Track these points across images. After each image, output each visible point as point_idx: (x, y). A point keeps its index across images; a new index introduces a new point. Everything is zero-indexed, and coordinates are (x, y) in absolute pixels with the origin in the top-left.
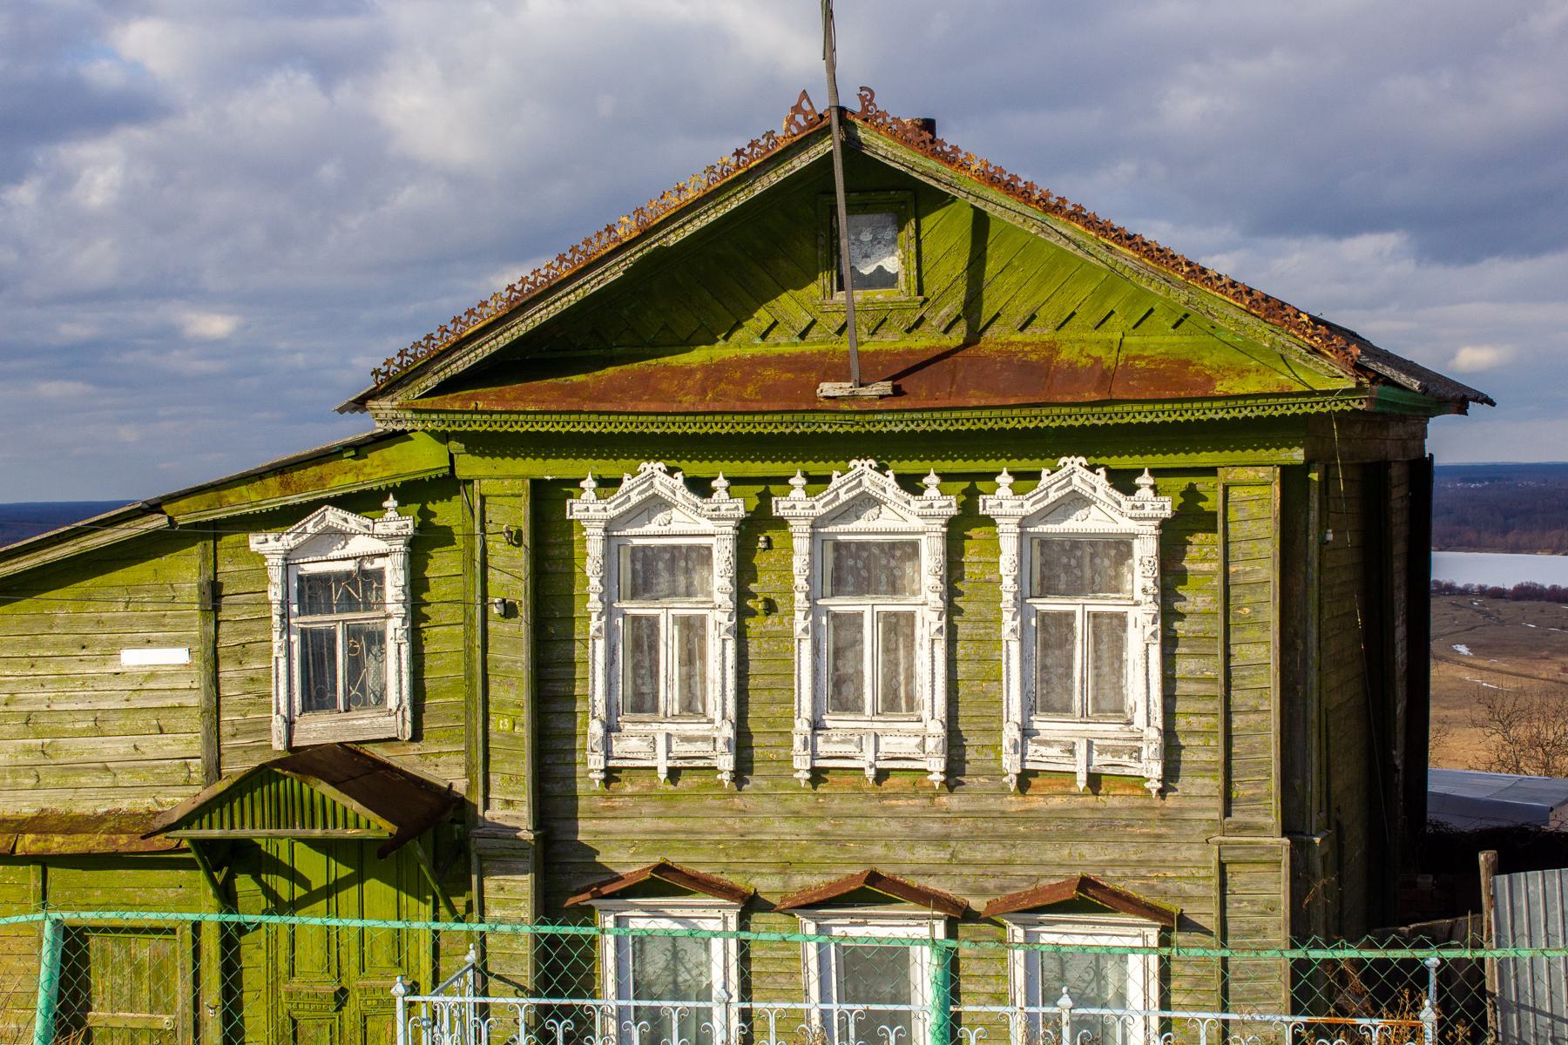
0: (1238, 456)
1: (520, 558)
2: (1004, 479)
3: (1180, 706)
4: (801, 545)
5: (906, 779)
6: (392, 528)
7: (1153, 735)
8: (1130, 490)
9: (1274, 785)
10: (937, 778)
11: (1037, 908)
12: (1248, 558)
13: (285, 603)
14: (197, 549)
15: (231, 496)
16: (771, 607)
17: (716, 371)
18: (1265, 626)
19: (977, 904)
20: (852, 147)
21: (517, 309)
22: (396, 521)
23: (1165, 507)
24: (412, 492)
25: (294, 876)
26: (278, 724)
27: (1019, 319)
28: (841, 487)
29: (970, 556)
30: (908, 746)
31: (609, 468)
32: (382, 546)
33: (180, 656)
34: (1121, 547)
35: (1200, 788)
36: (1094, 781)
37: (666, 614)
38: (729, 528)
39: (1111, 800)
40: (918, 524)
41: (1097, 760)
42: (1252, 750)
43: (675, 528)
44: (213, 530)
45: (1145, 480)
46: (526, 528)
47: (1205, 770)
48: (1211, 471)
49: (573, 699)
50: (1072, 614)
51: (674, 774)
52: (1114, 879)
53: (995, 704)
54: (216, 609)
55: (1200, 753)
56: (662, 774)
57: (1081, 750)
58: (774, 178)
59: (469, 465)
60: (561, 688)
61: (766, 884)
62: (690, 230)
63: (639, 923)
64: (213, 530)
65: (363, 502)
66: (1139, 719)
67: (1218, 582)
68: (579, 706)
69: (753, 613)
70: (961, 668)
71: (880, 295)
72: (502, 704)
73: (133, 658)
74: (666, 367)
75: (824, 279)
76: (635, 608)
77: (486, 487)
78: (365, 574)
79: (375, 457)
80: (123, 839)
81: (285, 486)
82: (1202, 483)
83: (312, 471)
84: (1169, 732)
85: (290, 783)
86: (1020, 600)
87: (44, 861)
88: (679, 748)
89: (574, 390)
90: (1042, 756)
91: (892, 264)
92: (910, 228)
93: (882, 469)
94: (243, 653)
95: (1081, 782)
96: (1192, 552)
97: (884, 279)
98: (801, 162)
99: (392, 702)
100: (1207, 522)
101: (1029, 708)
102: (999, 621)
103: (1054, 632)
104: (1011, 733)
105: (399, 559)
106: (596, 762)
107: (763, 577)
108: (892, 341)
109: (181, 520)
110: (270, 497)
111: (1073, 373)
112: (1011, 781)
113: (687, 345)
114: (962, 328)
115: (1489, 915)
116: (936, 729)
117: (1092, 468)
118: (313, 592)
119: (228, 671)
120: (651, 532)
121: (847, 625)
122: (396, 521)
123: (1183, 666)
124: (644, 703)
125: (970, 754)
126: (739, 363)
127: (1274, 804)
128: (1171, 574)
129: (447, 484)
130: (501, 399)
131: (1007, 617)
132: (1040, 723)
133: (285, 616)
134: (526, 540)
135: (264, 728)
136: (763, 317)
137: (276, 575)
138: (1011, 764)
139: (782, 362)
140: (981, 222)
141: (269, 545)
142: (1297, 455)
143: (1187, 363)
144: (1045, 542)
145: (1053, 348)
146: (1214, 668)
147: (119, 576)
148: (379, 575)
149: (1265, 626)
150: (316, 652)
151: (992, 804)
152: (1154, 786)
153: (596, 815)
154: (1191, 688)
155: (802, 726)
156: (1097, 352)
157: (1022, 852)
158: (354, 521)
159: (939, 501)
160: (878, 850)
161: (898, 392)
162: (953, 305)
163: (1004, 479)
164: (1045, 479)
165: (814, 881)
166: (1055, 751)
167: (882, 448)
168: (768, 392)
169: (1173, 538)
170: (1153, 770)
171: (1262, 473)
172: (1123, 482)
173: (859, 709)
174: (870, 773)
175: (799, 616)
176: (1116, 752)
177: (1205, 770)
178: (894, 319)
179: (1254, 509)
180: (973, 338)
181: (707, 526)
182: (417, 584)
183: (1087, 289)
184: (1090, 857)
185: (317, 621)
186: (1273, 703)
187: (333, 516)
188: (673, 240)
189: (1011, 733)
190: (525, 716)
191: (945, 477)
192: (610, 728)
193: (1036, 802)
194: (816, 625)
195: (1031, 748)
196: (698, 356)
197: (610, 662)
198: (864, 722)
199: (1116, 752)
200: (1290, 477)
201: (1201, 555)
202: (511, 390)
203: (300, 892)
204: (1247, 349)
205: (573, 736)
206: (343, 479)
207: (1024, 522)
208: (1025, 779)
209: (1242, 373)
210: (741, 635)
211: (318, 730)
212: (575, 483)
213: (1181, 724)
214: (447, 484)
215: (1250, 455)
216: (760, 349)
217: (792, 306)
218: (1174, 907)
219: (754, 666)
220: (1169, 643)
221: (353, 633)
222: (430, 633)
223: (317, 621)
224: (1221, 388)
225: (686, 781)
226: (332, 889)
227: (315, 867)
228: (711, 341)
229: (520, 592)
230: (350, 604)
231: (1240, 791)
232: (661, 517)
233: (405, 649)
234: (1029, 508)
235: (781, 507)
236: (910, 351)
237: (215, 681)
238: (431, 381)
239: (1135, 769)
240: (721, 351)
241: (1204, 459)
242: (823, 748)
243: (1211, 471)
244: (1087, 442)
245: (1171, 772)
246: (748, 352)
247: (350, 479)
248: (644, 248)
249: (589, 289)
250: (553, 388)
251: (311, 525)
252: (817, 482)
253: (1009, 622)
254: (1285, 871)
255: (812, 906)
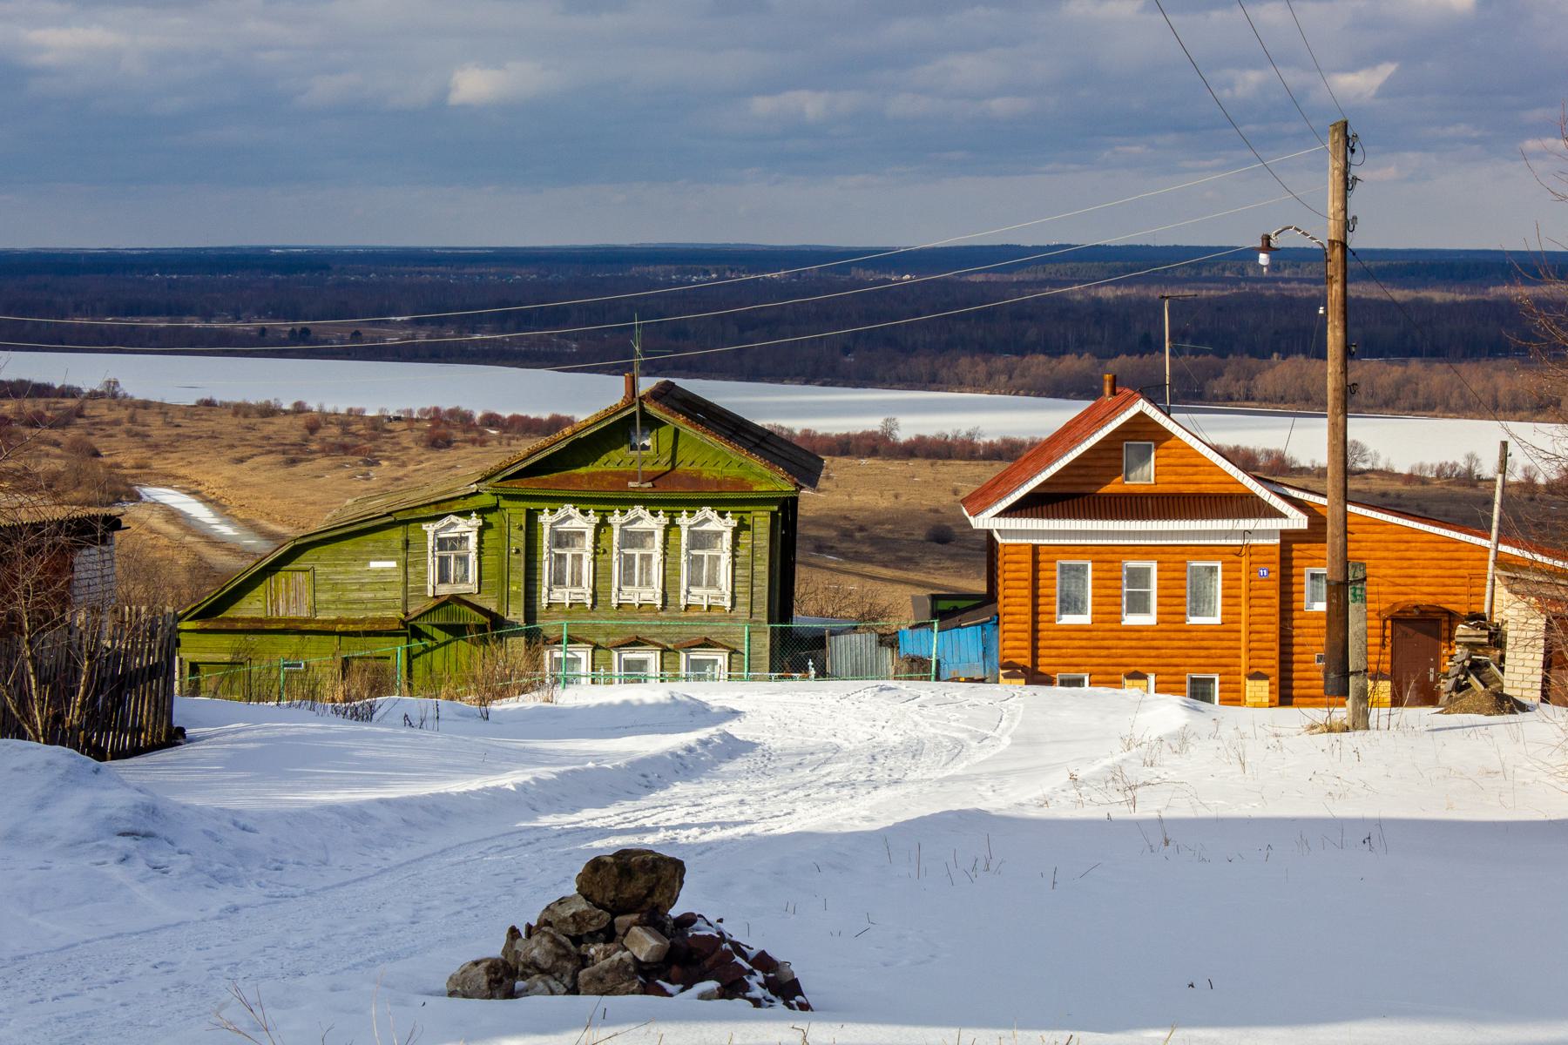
0: (757, 508)
1: (522, 534)
2: (685, 513)
3: (736, 584)
4: (616, 533)
5: (648, 607)
6: (474, 523)
7: (728, 594)
8: (724, 518)
9: (766, 608)
10: (659, 606)
11: (689, 647)
12: (759, 539)
13: (434, 547)
14: (401, 528)
15: (417, 511)
16: (605, 552)
17: (592, 476)
18: (764, 560)
19: (670, 646)
20: (642, 409)
21: (530, 455)
22: (475, 521)
23: (735, 523)
24: (482, 511)
25: (432, 639)
26: (430, 588)
27: (689, 463)
28: (631, 514)
29: (671, 536)
30: (650, 596)
31: (553, 506)
32: (470, 529)
33: (393, 564)
34: (719, 534)
35: (742, 610)
36: (709, 607)
37: (569, 553)
38: (593, 526)
39: (714, 613)
40: (655, 526)
41: (711, 601)
42: (759, 598)
43: (573, 526)
44: (406, 522)
45: (729, 515)
46: (524, 525)
47: (744, 604)
48: (749, 512)
49: (536, 580)
50: (703, 556)
51: (571, 605)
52: (713, 638)
53: (678, 583)
54: (407, 548)
55: (741, 599)
56: (567, 605)
57: (705, 598)
58: (616, 418)
59: (503, 503)
60: (532, 577)
61: (601, 640)
62: (588, 433)
63: (557, 654)
64: (406, 522)
65: (465, 514)
66: (724, 589)
67: (750, 546)
68: (538, 583)
69: (598, 553)
70: (667, 572)
71: (644, 453)
72: (513, 582)
73: (374, 565)
74: (574, 474)
75: (626, 447)
76: (558, 551)
77: (511, 511)
78: (461, 537)
79: (470, 499)
80: (377, 626)
81: (437, 509)
82: (745, 515)
83: (448, 504)
84: (733, 593)
85: (455, 607)
86: (687, 550)
87: (341, 634)
88: (573, 597)
89: (546, 481)
90: (692, 600)
91: (648, 442)
92: (655, 432)
93: (645, 509)
94: (414, 564)
95: (705, 608)
96: (742, 536)
97: (645, 448)
98: (625, 414)
99: (470, 581)
100: (747, 528)
101: (690, 584)
102: (680, 557)
103: (696, 562)
104: (683, 592)
105: (476, 533)
106: (545, 601)
107: (602, 542)
108: (647, 468)
109: (398, 519)
110: (433, 512)
111: (708, 482)
112: (683, 608)
113: (579, 466)
114: (670, 464)
115: (828, 649)
116: (660, 591)
117: (713, 511)
118: (442, 544)
119: (410, 570)
120: (566, 527)
121: (631, 558)
122: (475, 521)
123: (738, 572)
124: (630, 582)
125: (669, 599)
126: (597, 473)
127: (766, 614)
128: (735, 544)
129: (495, 508)
130: (522, 484)
131: (683, 556)
132: (692, 589)
133: (433, 552)
134: (524, 528)
135: (426, 589)
136: (604, 458)
137: (431, 537)
138: (683, 602)
139: (611, 473)
140: (677, 432)
141: (430, 528)
142: (776, 508)
143: (743, 479)
144: (694, 532)
145: (700, 473)
146: (748, 572)
147: (369, 537)
148: (467, 538)
149: (764, 560)
150: (444, 562)
151: (676, 615)
152: (728, 609)
153: (543, 618)
154: (740, 579)
155: (615, 590)
156: (714, 474)
157: (685, 630)
158: (461, 520)
159: (663, 519)
160: (639, 629)
161: (654, 486)
162: (668, 458)
163: (685, 513)
164: (629, 512)
165: (618, 639)
166: (697, 598)
167: (645, 503)
168: (611, 484)
169: (736, 533)
170: (728, 604)
171: (765, 513)
172: (722, 515)
173: (634, 585)
174: (637, 605)
175: (614, 555)
176: (717, 598)
177: (744, 604)
178: (649, 461)
179: (762, 524)
180: (673, 468)
181: (585, 525)
182: (480, 542)
183: (711, 454)
184: (707, 631)
185: (444, 553)
186: (766, 583)
187: (453, 518)
188: (582, 436)
189: (683, 592)
190: (522, 586)
191: (665, 512)
192: (550, 590)
193: (690, 614)
194: (550, 558)
195: (689, 597)
196: (583, 470)
197: (550, 568)
198: (636, 588)
199: (717, 598)
200: (773, 514)
201: (745, 538)
202: (525, 480)
203: (435, 644)
204: (761, 475)
205: (536, 593)
206: (458, 507)
207: (622, 525)
208: (687, 607)
209: (761, 484)
210: (595, 560)
211: (444, 590)
212: (542, 510)
213: (737, 590)
214: (495, 508)
215: (761, 508)
216: (603, 468)
217: (614, 455)
218: (733, 646)
219: (598, 571)
220: (734, 564)
221: (643, 557)
222: (484, 558)
223: (444, 553)
224: (755, 489)
225: (574, 607)
226: (446, 643)
227: (441, 636)
228: (587, 465)
229: (522, 546)
230: (453, 548)
231: (755, 610)
232: (569, 522)
233: (476, 563)
234: (692, 523)
235: (610, 520)
236: (654, 472)
237: (406, 573)
238: (499, 478)
239: (721, 603)
240: (590, 469)
241: (747, 508)
242: (622, 597)
243: (749, 512)
244: (575, 501)
245: (733, 605)
246: (600, 470)
247: (461, 506)
248: (1082, 476)
249: (554, 450)
250: (538, 480)
251: (445, 522)
252: (624, 512)
253: (684, 558)
254: (768, 634)
255: (618, 647)
